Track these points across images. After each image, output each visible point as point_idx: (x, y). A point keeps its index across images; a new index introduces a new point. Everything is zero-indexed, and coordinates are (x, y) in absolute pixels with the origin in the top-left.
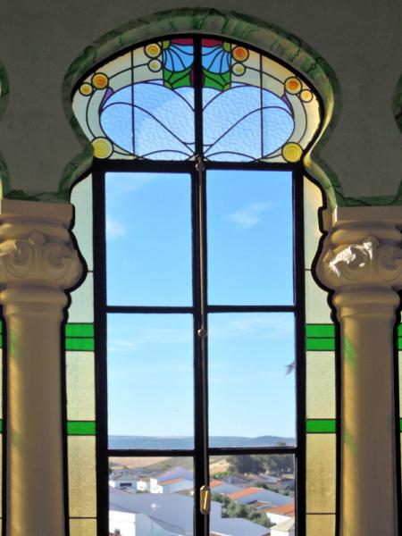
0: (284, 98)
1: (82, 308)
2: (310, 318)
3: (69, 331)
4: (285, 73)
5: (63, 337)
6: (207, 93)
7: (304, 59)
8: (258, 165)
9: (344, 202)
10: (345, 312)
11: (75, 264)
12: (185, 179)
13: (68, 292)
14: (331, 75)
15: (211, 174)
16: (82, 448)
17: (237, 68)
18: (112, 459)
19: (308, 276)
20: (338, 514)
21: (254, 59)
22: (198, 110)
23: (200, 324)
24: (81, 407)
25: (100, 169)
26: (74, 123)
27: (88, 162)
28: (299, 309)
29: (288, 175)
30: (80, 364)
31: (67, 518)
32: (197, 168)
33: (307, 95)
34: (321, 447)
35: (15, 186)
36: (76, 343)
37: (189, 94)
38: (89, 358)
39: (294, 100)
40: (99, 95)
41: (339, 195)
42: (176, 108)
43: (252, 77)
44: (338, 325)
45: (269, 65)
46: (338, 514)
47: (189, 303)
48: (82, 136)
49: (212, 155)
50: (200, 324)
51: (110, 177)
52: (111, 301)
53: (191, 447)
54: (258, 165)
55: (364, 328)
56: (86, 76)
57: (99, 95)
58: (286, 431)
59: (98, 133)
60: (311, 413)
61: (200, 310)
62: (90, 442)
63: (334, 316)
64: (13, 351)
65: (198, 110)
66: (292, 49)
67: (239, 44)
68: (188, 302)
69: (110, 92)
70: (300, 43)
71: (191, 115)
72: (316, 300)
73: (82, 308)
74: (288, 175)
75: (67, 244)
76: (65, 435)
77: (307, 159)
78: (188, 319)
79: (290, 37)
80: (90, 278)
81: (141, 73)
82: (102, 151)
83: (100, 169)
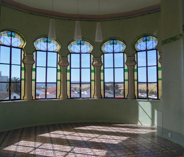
0: (89, 46)
1: (68, 68)
2: (92, 69)
3: (67, 70)
4: (89, 44)
5: (67, 71)
6: (48, 43)
7: (91, 42)
8: (53, 52)
9: (27, 54)
10: (95, 69)
11: (68, 63)
12: (46, 52)
13: (67, 66)
14: (93, 44)
15: (82, 54)
16: (68, 83)
17: (51, 41)
18: (105, 84)
19: (92, 65)
20: (95, 90)
21: (86, 42)
22: (81, 47)
23: (80, 70)
24: (68, 78)
25: (36, 51)
26: (68, 49)
27: (103, 53)
28: (90, 68)
29: (90, 54)
30: (68, 74)
31: (128, 90)
32: (80, 53)
33: (92, 46)
34: (59, 83)
35: (62, 56)
36: (68, 72)
37: (80, 46)
38: (69, 73)
39: (90, 46)
40: (71, 46)
41: (26, 53)
42: (78, 47)
43: (86, 44)
44: (94, 70)
45: (88, 42)
46: (95, 90)
47: (113, 67)
48: (35, 48)
49: (82, 52)
50: (80, 70)
51: (71, 54)
52: (105, 67)
53: (148, 83)
54: (53, 52)
55: (97, 70)
56: (102, 45)
57: (71, 46)
58: (55, 81)
59: (36, 47)
60: (92, 79)
61: (47, 67)
62: (137, 82)
63: (94, 69)
64: (62, 73)
65: (81, 47)
66: (90, 42)
67: (85, 40)
68: (79, 67)
69: (72, 45)
70: (91, 41)
71: (80, 48)
72: (59, 66)
73: (68, 68)
74: (90, 54)
75: (32, 59)
76: (67, 81)
77: (58, 51)
78: (79, 69)
79: (90, 40)
80: (69, 65)
81: (75, 44)
82: (37, 49)
83: (70, 53)
